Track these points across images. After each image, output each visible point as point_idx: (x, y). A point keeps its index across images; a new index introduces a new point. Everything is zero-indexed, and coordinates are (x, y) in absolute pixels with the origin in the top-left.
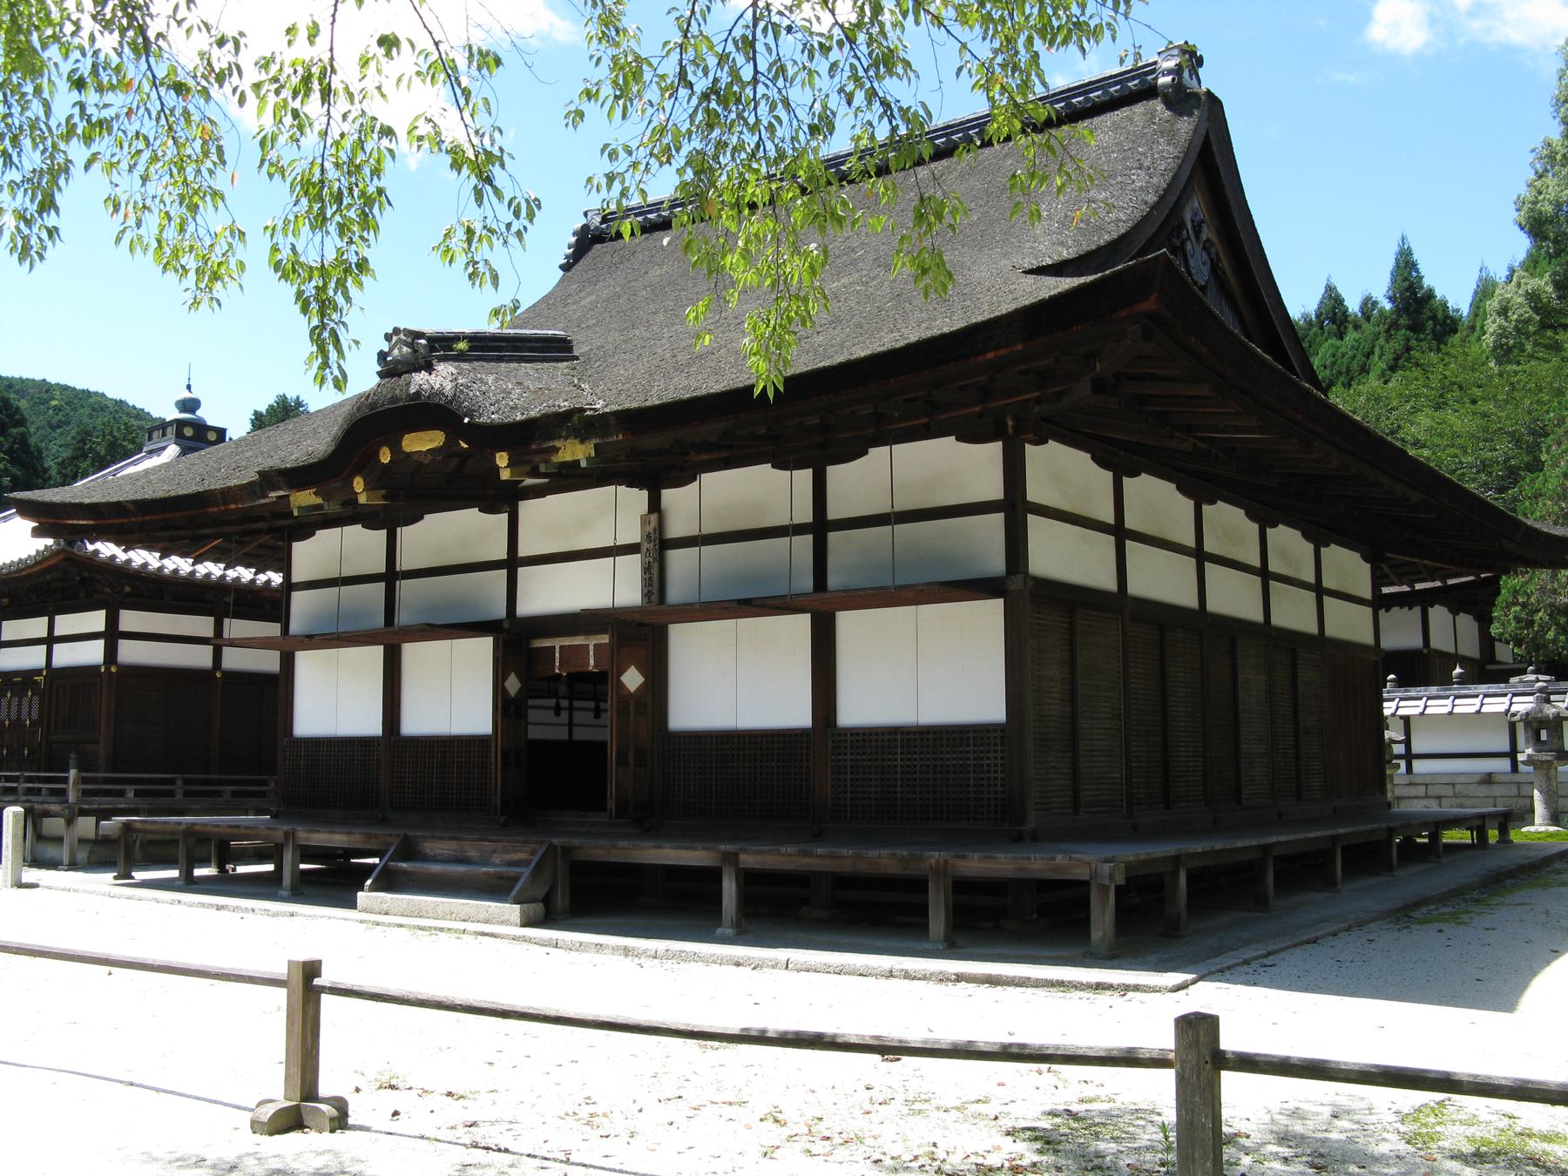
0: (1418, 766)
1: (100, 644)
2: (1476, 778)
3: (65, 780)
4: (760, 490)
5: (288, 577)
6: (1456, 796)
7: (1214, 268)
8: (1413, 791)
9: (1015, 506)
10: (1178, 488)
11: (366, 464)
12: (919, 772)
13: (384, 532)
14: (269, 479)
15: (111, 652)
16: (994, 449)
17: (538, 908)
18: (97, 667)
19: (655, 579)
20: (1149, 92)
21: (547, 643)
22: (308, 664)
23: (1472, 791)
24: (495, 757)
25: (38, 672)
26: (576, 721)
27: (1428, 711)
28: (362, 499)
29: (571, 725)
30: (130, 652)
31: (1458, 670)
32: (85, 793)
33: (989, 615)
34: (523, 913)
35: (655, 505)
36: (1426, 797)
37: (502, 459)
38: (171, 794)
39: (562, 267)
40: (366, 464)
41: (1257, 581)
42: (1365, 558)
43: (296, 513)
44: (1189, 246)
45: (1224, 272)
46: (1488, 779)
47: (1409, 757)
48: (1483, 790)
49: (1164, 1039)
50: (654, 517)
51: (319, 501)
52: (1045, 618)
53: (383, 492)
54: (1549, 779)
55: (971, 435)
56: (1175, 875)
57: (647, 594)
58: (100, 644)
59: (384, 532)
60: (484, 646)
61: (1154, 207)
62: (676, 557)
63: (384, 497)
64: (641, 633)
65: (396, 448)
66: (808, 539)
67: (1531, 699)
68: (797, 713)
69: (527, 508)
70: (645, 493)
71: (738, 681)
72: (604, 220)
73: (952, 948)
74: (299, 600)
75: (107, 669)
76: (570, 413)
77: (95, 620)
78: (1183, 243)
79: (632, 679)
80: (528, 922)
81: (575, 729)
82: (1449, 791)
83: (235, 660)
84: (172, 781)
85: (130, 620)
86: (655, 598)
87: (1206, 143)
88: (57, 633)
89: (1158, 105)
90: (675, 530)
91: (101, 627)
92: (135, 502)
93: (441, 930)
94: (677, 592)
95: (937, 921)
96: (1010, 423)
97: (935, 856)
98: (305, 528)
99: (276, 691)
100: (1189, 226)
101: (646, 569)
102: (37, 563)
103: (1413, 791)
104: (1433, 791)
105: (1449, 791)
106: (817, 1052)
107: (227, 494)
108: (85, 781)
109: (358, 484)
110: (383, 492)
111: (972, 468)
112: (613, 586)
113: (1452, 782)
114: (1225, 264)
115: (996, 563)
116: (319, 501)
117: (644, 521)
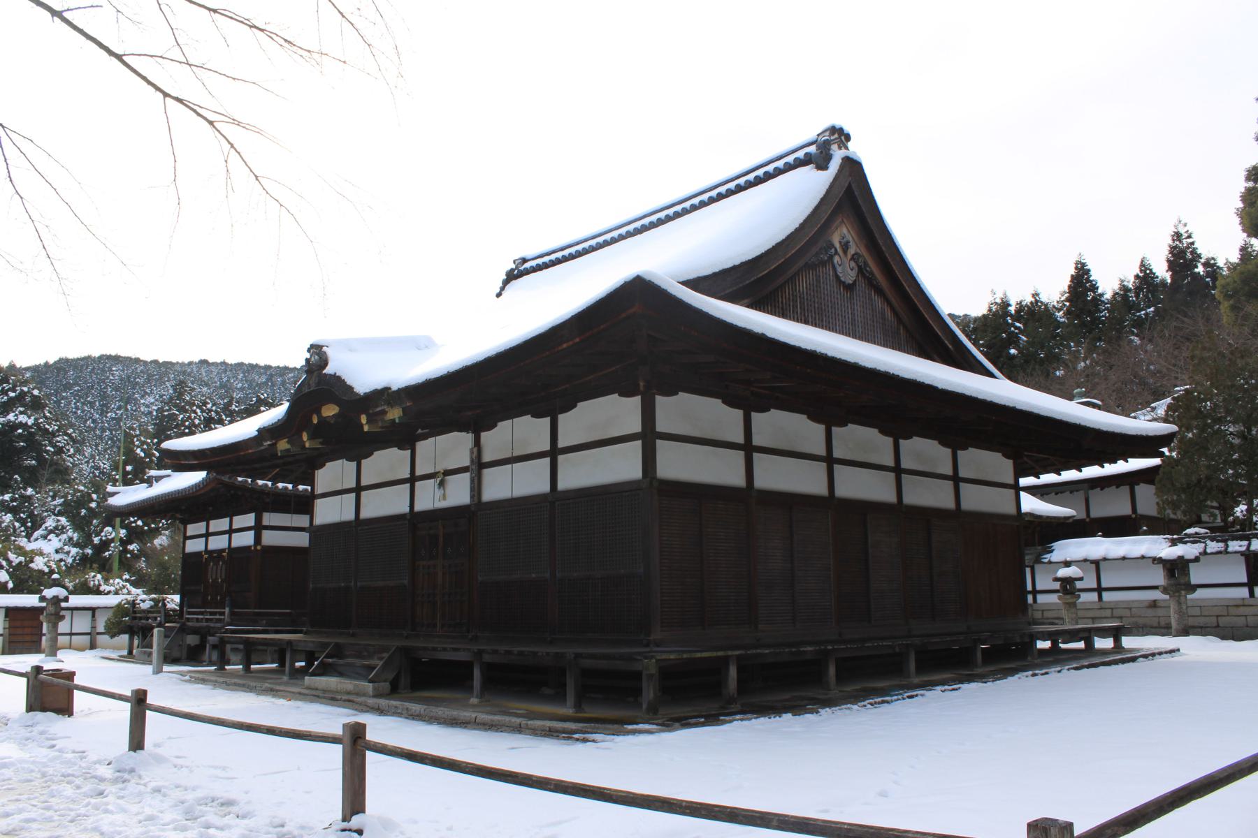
0: (1107, 596)
1: (252, 533)
3: (223, 614)
5: (313, 489)
6: (1132, 616)
7: (861, 271)
10: (809, 418)
11: (306, 424)
15: (258, 538)
17: (386, 686)
18: (249, 547)
25: (223, 550)
28: (307, 445)
30: (269, 538)
34: (374, 689)
35: (477, 443)
37: (364, 419)
40: (306, 424)
41: (892, 475)
42: (1006, 456)
44: (836, 259)
45: (872, 273)
46: (1154, 604)
47: (1035, 592)
48: (1150, 612)
49: (338, 731)
54: (1180, 604)
57: (472, 497)
58: (252, 533)
66: (547, 460)
69: (422, 446)
74: (320, 504)
77: (249, 519)
78: (831, 257)
82: (1127, 613)
85: (269, 518)
87: (849, 190)
88: (211, 530)
90: (487, 458)
95: (649, 693)
96: (642, 384)
97: (570, 651)
100: (837, 245)
101: (472, 481)
102: (205, 486)
104: (1116, 613)
105: (1127, 613)
106: (1138, 831)
109: (305, 437)
113: (1128, 606)
114: (873, 266)
117: (472, 452)
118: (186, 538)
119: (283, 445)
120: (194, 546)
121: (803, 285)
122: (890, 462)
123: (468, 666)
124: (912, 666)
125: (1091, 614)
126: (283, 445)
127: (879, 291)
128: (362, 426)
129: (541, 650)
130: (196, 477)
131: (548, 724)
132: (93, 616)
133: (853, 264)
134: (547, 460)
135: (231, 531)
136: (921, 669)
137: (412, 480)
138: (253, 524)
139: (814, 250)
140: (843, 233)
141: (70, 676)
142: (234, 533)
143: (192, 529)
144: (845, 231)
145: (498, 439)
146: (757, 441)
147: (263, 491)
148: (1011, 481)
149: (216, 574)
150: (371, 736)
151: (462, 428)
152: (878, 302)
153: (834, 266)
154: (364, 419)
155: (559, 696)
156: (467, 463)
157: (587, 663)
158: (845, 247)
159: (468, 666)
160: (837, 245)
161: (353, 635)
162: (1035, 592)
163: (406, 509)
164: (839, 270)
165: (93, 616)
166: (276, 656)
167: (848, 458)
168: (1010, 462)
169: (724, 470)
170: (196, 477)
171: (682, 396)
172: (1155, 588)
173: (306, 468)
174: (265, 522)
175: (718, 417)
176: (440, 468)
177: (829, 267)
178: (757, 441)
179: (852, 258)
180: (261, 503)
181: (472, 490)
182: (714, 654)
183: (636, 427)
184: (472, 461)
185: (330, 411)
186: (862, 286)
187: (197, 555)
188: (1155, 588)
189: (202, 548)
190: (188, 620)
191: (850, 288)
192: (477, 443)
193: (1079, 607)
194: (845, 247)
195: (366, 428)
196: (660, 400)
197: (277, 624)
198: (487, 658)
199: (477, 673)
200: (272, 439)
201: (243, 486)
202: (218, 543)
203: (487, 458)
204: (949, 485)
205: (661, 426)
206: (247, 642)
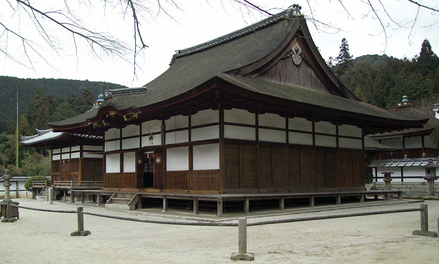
2: (420, 183)
6: (414, 188)
8: (403, 186)
14: (88, 120)
15: (81, 155)
17: (134, 207)
21: (147, 153)
23: (419, 186)
24: (136, 176)
26: (150, 168)
27: (413, 165)
29: (148, 169)
30: (86, 155)
31: (424, 154)
35: (163, 124)
36: (407, 188)
37: (125, 117)
38: (94, 185)
39: (170, 65)
43: (94, 127)
44: (293, 56)
47: (377, 178)
48: (422, 186)
49: (76, 210)
50: (163, 126)
51: (98, 125)
53: (109, 123)
56: (245, 201)
57: (162, 142)
60: (134, 153)
63: (109, 124)
65: (109, 114)
67: (427, 162)
71: (176, 163)
75: (81, 158)
76: (131, 108)
77: (78, 148)
78: (291, 55)
79: (158, 160)
81: (150, 170)
82: (413, 186)
83: (265, 136)
84: (94, 183)
85: (85, 148)
86: (163, 143)
90: (167, 129)
91: (79, 150)
93: (234, 219)
96: (219, 106)
98: (107, 128)
99: (102, 163)
101: (162, 137)
103: (403, 186)
104: (408, 186)
105: (413, 186)
107: (82, 123)
110: (109, 123)
111: (212, 115)
113: (413, 184)
115: (217, 136)
116: (98, 125)
118: (52, 155)
122: (311, 131)
124: (313, 203)
125: (398, 186)
126: (95, 124)
127: (310, 66)
128: (124, 119)
131: (187, 217)
132: (17, 184)
133: (300, 57)
136: (316, 205)
137: (141, 136)
138: (79, 150)
139: (285, 53)
140: (296, 46)
143: (55, 151)
144: (297, 44)
145: (170, 122)
146: (260, 124)
147: (87, 139)
148: (361, 136)
151: (159, 119)
152: (309, 70)
153: (292, 58)
154: (125, 117)
155: (191, 210)
157: (200, 199)
158: (297, 51)
159: (162, 200)
160: (294, 50)
162: (377, 178)
164: (294, 60)
165: (17, 184)
166: (92, 198)
167: (296, 129)
168: (361, 129)
169: (248, 135)
171: (234, 109)
172: (422, 177)
173: (102, 131)
174: (84, 149)
175: (248, 117)
176: (151, 132)
177: (290, 59)
178: (260, 124)
179: (300, 55)
180: (82, 142)
183: (217, 120)
184: (162, 130)
185: (112, 113)
186: (303, 66)
187: (58, 161)
188: (422, 177)
190: (56, 185)
191: (298, 66)
192: (163, 124)
193: (435, 184)
194: (297, 51)
195: (125, 120)
196: (226, 111)
200: (92, 122)
201: (76, 136)
202: (66, 157)
203: (167, 129)
204: (334, 138)
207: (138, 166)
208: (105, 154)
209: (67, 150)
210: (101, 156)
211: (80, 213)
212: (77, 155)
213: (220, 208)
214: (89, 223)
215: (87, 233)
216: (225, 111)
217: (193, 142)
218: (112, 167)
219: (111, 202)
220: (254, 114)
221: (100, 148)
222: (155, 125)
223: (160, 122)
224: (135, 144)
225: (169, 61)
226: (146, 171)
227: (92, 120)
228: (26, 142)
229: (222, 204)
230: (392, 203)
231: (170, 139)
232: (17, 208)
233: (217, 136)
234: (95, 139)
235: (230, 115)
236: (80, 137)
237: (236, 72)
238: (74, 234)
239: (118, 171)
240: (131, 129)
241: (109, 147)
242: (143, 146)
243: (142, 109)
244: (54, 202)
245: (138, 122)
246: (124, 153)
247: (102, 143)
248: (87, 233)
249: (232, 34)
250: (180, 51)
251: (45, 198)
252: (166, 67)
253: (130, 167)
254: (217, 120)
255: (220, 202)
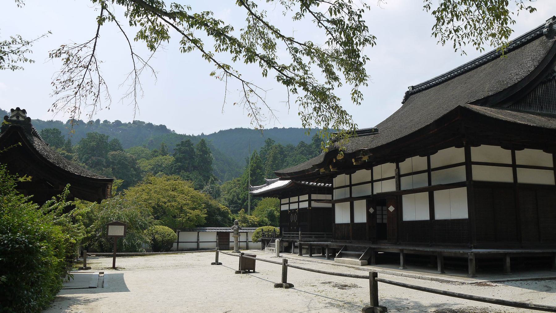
3: (298, 234)
4: (417, 162)
5: (332, 185)
9: (468, 163)
10: (545, 151)
11: (331, 162)
12: (432, 230)
13: (473, 166)
14: (315, 166)
15: (310, 204)
16: (463, 149)
19: (398, 185)
20: (541, 35)
22: (337, 206)
25: (296, 209)
32: (303, 237)
33: (463, 191)
35: (398, 167)
37: (353, 160)
38: (323, 237)
40: (331, 162)
49: (367, 274)
52: (478, 192)
55: (458, 146)
57: (397, 188)
59: (473, 166)
61: (533, 72)
62: (402, 179)
64: (396, 198)
66: (427, 174)
68: (427, 217)
69: (375, 168)
70: (395, 164)
71: (414, 211)
72: (413, 89)
73: (405, 268)
77: (306, 197)
80: (363, 265)
84: (323, 234)
85: (314, 196)
89: (544, 38)
90: (402, 173)
92: (294, 173)
94: (403, 188)
98: (335, 175)
99: (331, 212)
108: (303, 234)
109: (331, 167)
111: (456, 154)
112: (389, 187)
115: (464, 178)
117: (396, 171)
118: (281, 204)
119: (322, 170)
120: (284, 208)
121: (540, 91)
123: (398, 255)
126: (322, 170)
129: (428, 249)
130: (286, 182)
134: (427, 174)
135: (299, 202)
141: (255, 256)
142: (301, 203)
145: (407, 165)
147: (316, 187)
149: (294, 218)
150: (380, 276)
154: (353, 160)
156: (394, 175)
159: (398, 255)
161: (351, 243)
163: (370, 194)
169: (504, 176)
170: (286, 182)
173: (330, 178)
174: (312, 198)
175: (501, 154)
181: (397, 185)
182: (523, 251)
183: (463, 160)
187: (286, 211)
188: (292, 267)
189: (287, 208)
192: (398, 167)
195: (354, 164)
197: (319, 238)
198: (405, 252)
199: (401, 257)
201: (304, 185)
202: (294, 206)
203: (402, 173)
205: (473, 159)
206: (311, 246)
207: (369, 215)
208: (333, 202)
209: (295, 199)
210: (330, 205)
211: (374, 279)
212: (305, 205)
213: (472, 267)
214: (293, 276)
215: (291, 286)
216: (472, 148)
217: (435, 186)
218: (342, 217)
219: (341, 256)
220: (510, 151)
221: (329, 197)
222: (388, 169)
223: (394, 165)
224: (367, 190)
225: (402, 99)
226: (379, 221)
227: (319, 166)
228: (255, 192)
229: (474, 262)
230: (357, 247)
231: (406, 183)
232: (254, 261)
233: (464, 178)
234: (324, 187)
235: (480, 153)
236: (308, 185)
237: (483, 102)
238: (278, 286)
239: (427, 217)
240: (362, 175)
241: (337, 194)
242: (375, 193)
243: (371, 150)
244: (281, 254)
245: (369, 166)
246: (403, 196)
247: (330, 191)
248: (291, 286)
249: (460, 68)
250: (413, 87)
251: (273, 250)
252: (397, 105)
253: (361, 217)
254: (463, 160)
255: (471, 260)
